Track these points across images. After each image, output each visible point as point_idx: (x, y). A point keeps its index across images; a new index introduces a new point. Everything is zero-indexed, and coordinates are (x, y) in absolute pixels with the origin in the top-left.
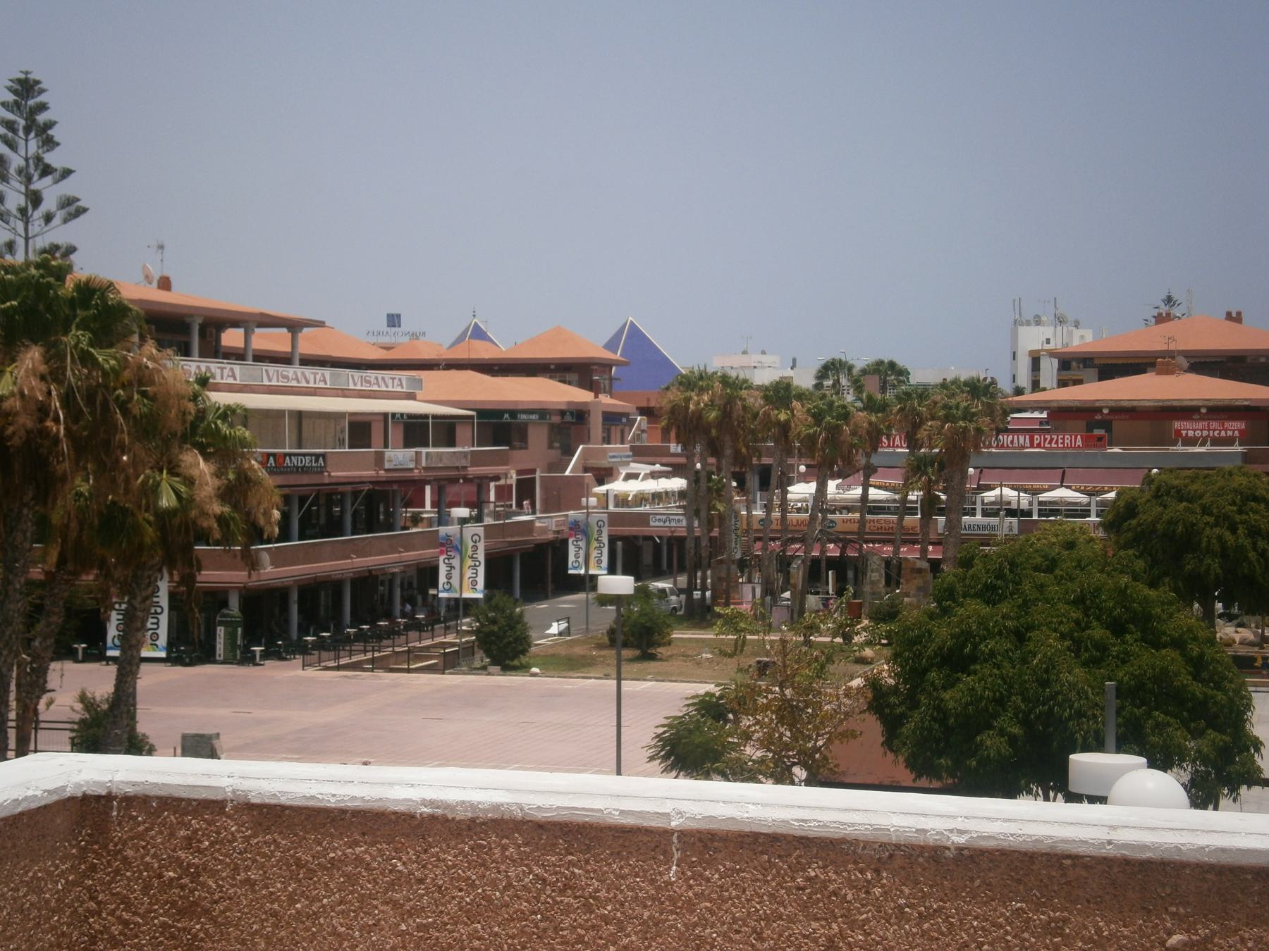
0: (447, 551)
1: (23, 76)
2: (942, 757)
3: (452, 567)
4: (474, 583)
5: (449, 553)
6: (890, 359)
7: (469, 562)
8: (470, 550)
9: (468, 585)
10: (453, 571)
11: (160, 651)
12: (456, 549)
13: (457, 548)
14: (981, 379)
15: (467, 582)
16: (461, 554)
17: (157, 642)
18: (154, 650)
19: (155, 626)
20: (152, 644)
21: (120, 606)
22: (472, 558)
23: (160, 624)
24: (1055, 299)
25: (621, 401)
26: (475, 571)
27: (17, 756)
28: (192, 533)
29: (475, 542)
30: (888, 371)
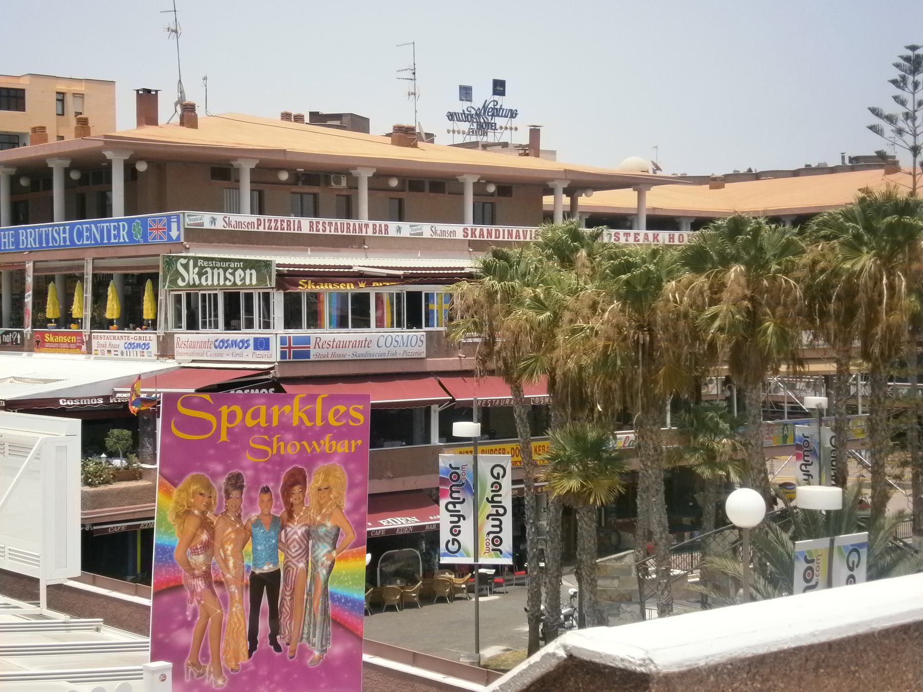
1: (910, 53)
3: (461, 517)
4: (497, 542)
7: (488, 509)
8: (489, 489)
10: (462, 523)
11: (505, 557)
12: (464, 486)
13: (815, 453)
15: (484, 539)
16: (475, 495)
18: (498, 557)
19: (498, 529)
20: (493, 550)
21: (455, 507)
22: (492, 501)
26: (497, 523)
27: (870, 578)
29: (498, 478)
30: (898, 162)
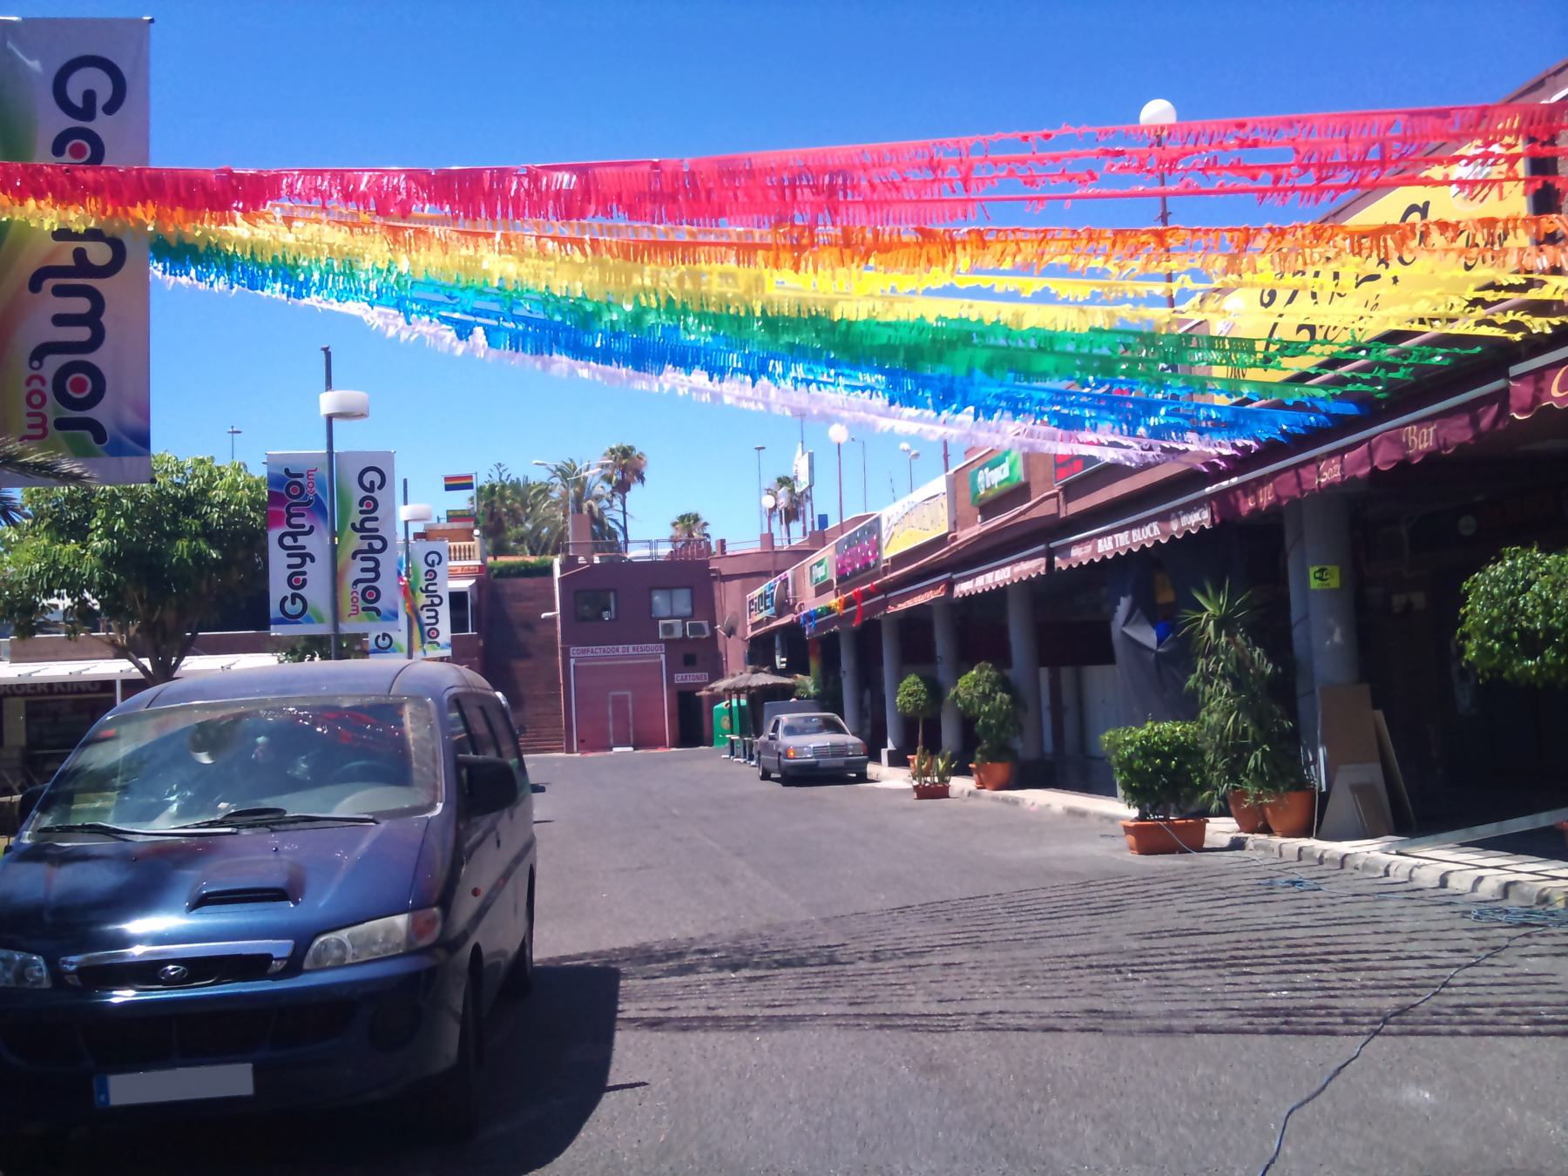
0: (291, 516)
2: (531, 624)
3: (306, 557)
5: (294, 521)
6: (270, 461)
9: (354, 602)
14: (897, 403)
17: (94, 413)
20: (61, 424)
23: (105, 319)
24: (405, 481)
25: (880, 662)
26: (371, 564)
28: (472, 318)
